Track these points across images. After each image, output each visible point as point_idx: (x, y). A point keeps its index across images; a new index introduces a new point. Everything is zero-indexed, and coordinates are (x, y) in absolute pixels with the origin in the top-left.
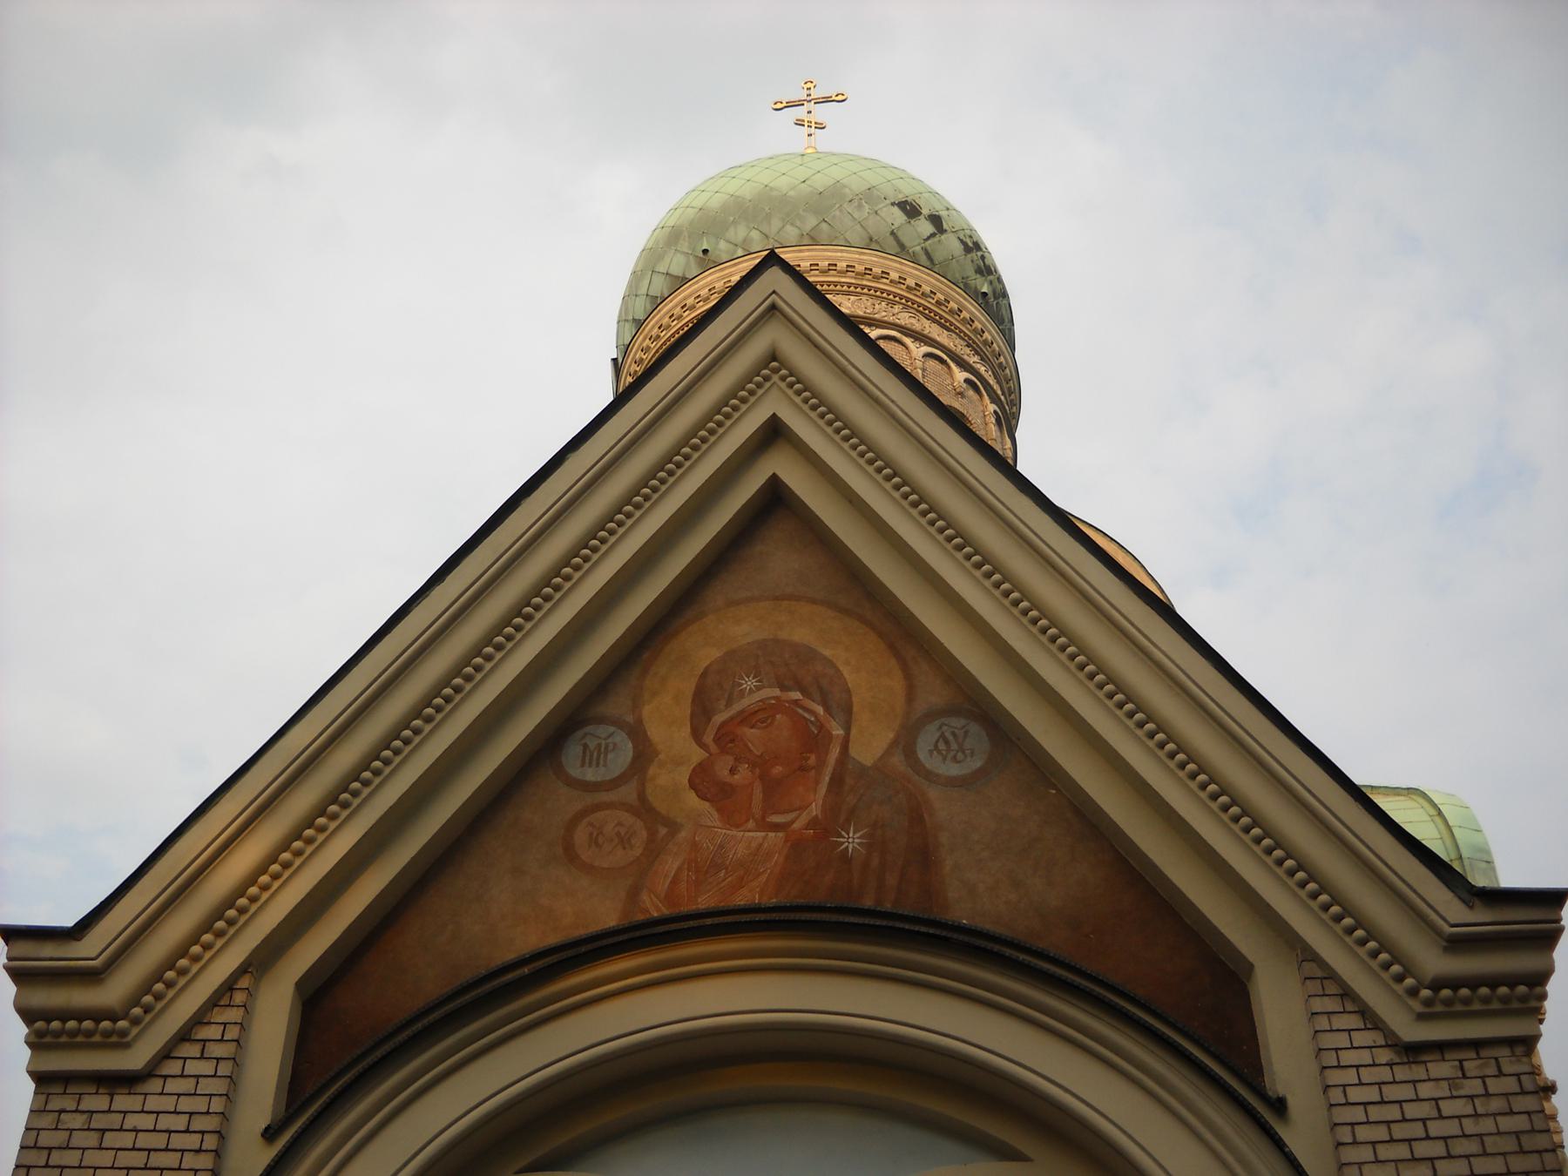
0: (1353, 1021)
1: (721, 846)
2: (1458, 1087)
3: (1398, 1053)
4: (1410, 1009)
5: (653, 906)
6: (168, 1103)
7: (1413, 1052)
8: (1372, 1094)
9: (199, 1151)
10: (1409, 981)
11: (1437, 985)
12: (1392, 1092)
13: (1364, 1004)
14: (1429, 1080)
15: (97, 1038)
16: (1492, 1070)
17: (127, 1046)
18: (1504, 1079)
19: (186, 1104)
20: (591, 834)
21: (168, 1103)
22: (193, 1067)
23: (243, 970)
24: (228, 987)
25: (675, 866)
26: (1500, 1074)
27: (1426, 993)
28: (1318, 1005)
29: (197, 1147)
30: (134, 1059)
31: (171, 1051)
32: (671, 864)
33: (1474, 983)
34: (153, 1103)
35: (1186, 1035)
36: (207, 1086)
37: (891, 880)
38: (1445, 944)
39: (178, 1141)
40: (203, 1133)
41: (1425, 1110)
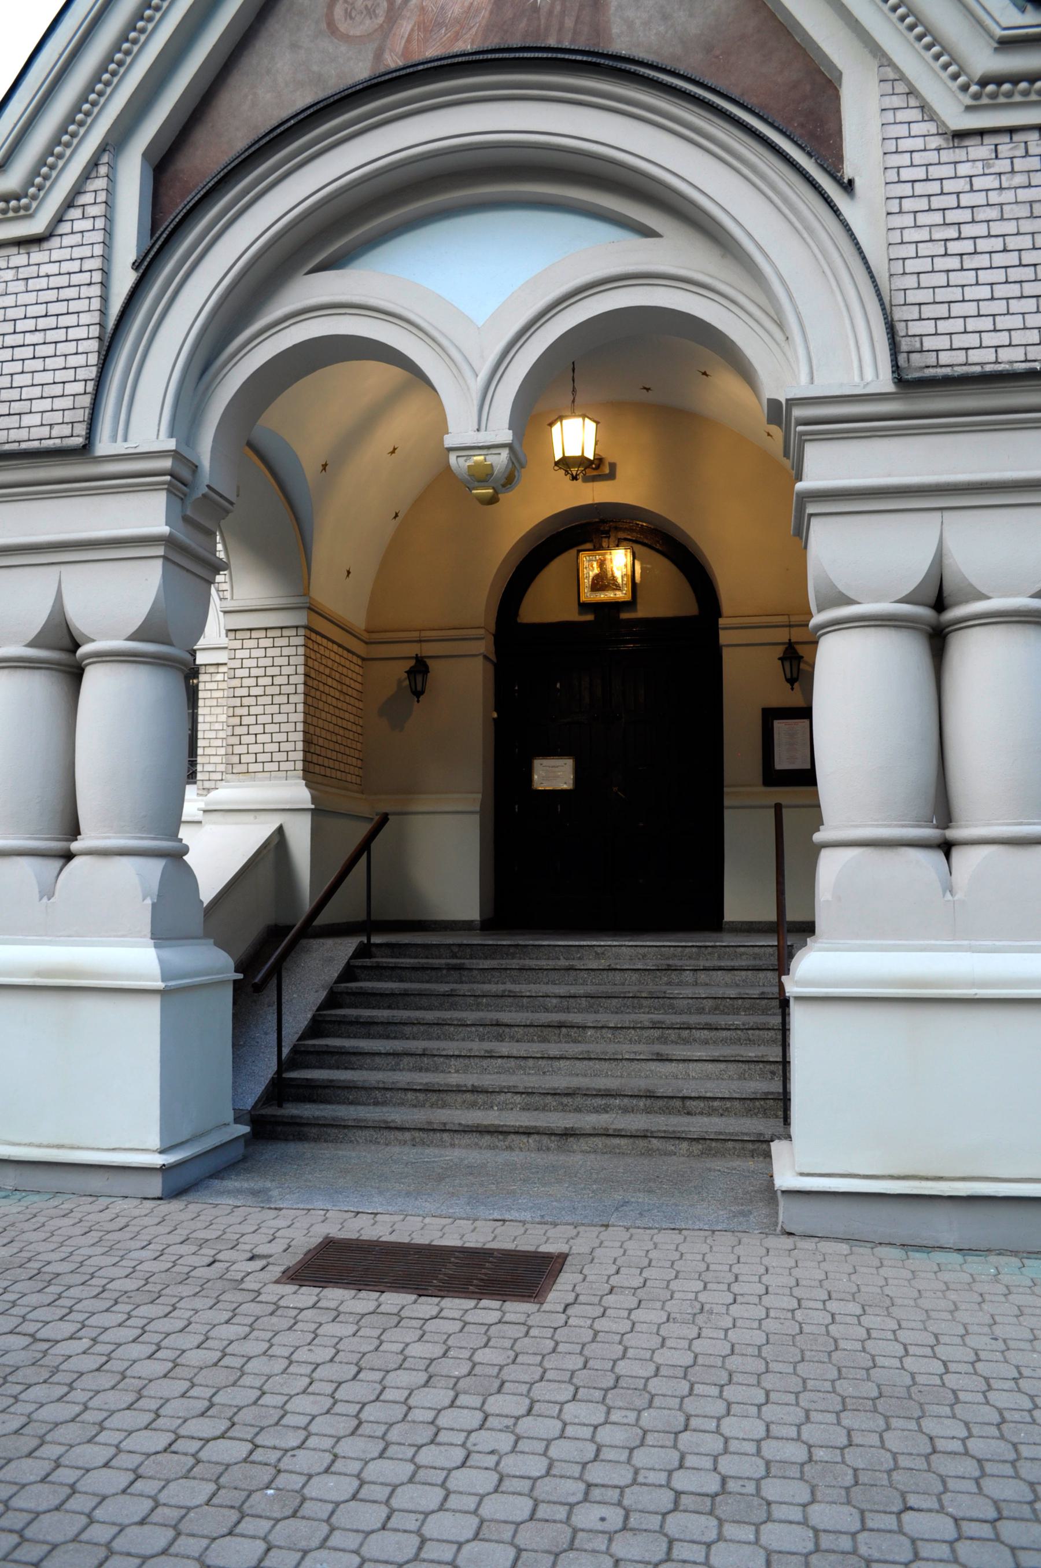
0: (915, 114)
1: (442, 8)
2: (989, 167)
3: (947, 140)
4: (960, 101)
5: (393, 60)
6: (65, 254)
7: (960, 135)
8: (920, 173)
9: (90, 284)
10: (962, 79)
11: (983, 82)
12: (935, 172)
13: (923, 99)
14: (968, 161)
15: (11, 214)
16: (1021, 152)
17: (31, 216)
18: (1029, 159)
19: (77, 253)
20: (346, 10)
21: (65, 254)
22: (79, 225)
23: (102, 149)
24: (94, 163)
25: (409, 28)
26: (1027, 154)
27: (974, 88)
28: (888, 102)
29: (88, 282)
30: (37, 226)
31: (62, 216)
32: (405, 27)
33: (1015, 79)
34: (56, 255)
35: (772, 125)
36: (88, 265)
37: (569, 23)
38: (996, 45)
39: (76, 279)
40: (91, 271)
41: (962, 185)
